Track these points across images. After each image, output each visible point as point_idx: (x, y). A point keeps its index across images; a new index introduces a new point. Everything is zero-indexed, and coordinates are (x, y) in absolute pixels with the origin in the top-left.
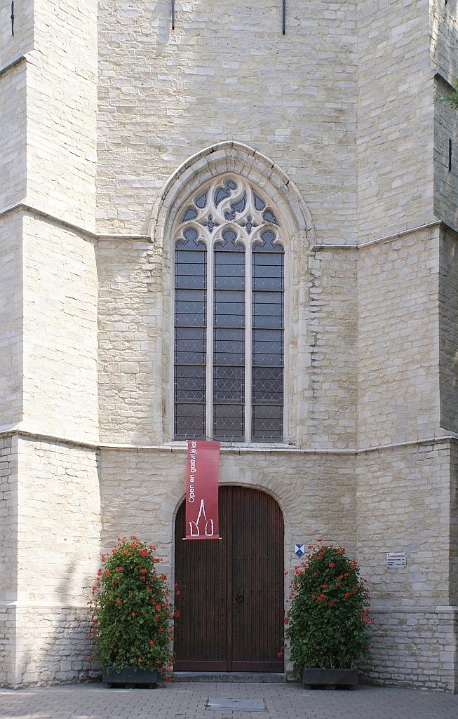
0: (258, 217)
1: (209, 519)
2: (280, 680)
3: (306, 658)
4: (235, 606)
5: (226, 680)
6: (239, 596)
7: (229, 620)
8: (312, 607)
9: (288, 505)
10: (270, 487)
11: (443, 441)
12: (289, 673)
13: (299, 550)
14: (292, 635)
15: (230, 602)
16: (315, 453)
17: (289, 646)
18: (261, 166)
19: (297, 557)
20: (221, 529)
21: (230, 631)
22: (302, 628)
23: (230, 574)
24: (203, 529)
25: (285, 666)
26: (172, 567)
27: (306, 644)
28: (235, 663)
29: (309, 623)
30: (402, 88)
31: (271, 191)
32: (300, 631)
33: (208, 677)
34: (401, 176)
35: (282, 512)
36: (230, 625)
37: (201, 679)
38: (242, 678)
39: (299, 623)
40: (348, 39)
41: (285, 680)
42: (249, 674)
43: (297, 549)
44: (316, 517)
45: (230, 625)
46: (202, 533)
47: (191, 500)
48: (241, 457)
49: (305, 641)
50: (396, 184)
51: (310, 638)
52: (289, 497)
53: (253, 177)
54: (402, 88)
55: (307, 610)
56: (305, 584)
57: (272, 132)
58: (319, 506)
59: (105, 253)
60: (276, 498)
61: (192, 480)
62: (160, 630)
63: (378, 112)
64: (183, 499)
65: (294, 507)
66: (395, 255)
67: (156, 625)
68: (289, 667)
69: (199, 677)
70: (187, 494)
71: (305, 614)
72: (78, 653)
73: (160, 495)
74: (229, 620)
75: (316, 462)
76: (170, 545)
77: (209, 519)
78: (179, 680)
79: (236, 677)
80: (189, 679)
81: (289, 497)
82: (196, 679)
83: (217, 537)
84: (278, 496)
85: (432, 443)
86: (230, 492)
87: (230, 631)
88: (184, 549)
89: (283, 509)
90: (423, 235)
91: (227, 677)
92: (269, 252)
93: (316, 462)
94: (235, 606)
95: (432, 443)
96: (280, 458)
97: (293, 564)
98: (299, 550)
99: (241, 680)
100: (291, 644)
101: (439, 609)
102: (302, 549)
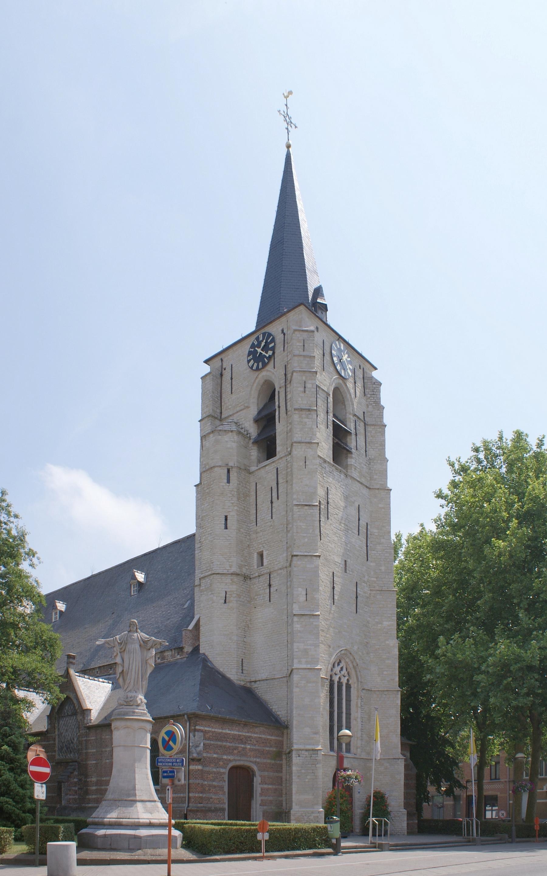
0: (346, 674)
11: (402, 759)
18: (351, 658)
30: (387, 642)
31: (351, 666)
34: (387, 671)
40: (369, 619)
50: (385, 673)
53: (347, 660)
54: (387, 642)
57: (38, 642)
59: (90, 747)
63: (378, 647)
66: (385, 696)
72: (360, 698)
85: (398, 759)
90: (395, 692)
92: (348, 686)
95: (398, 759)
101: (401, 810)
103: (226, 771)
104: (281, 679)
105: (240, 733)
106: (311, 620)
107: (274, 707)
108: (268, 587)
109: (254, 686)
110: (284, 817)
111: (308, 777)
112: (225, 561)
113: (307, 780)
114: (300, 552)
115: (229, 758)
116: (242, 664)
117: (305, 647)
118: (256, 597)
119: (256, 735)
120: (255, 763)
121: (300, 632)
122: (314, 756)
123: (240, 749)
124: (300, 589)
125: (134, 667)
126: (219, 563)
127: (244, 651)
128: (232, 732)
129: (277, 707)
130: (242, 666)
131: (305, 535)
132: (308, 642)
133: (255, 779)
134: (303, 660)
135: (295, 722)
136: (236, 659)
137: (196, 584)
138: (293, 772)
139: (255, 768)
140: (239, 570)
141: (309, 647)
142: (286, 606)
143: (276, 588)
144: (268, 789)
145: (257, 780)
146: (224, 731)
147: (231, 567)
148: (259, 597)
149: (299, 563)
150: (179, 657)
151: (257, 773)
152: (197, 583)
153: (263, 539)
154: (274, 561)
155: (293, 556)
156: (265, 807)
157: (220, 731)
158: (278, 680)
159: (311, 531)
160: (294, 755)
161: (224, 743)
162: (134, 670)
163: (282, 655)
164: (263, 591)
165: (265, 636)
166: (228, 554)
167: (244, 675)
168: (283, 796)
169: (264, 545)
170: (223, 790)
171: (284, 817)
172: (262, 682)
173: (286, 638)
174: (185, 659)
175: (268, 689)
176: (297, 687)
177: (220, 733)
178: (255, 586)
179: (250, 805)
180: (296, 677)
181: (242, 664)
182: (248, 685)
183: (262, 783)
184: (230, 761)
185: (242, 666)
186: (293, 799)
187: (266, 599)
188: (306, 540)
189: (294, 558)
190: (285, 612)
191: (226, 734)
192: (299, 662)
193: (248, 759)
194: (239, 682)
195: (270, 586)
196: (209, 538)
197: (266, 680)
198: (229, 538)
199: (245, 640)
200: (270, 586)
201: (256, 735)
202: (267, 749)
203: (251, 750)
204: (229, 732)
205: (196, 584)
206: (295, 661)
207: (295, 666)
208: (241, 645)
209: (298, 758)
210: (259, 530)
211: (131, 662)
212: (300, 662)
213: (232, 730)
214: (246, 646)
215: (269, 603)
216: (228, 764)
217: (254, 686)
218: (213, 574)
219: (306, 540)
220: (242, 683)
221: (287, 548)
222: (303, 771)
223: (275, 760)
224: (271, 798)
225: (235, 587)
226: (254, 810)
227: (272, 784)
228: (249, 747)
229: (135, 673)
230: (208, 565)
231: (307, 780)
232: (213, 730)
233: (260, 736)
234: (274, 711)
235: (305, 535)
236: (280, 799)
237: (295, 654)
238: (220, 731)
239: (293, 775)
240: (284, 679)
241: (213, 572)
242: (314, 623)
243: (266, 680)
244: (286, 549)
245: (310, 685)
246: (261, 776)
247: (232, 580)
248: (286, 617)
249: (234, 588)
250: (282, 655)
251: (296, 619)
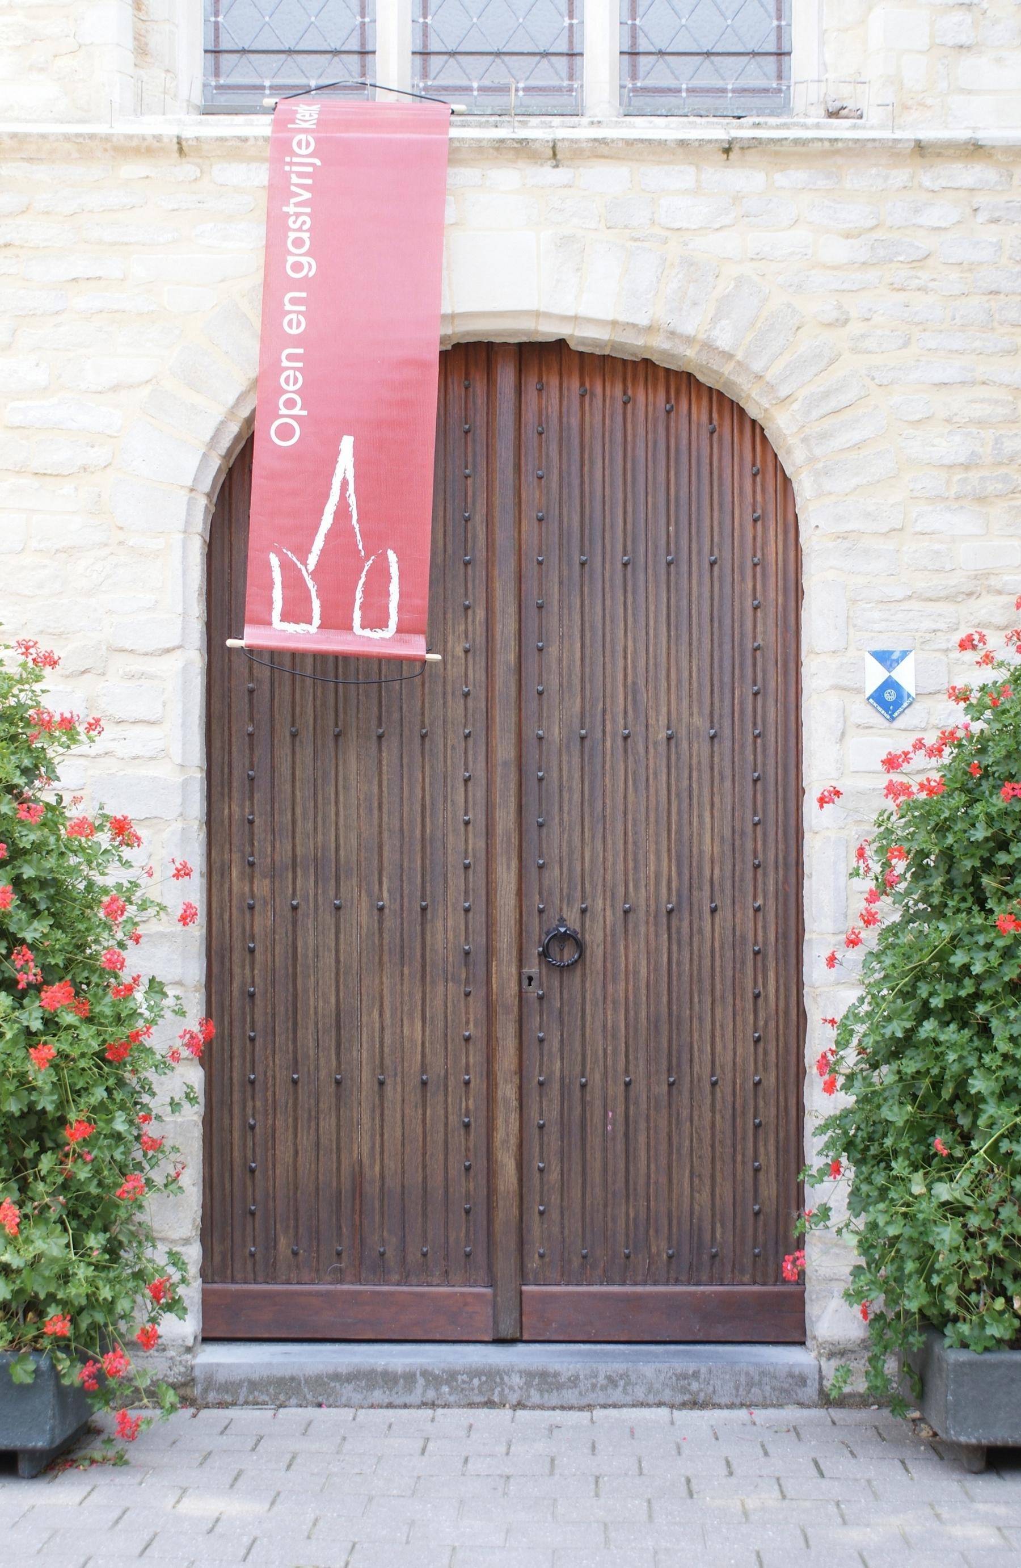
1: (376, 542)
2: (788, 1390)
3: (952, 1290)
4: (534, 991)
5: (486, 1393)
6: (563, 938)
7: (506, 1060)
8: (988, 987)
9: (824, 436)
10: (724, 340)
12: (837, 1352)
13: (890, 684)
14: (864, 1146)
15: (505, 974)
16: (975, 150)
17: (840, 1215)
19: (875, 717)
20: (434, 621)
21: (507, 1127)
22: (925, 1119)
23: (505, 819)
24: (348, 601)
25: (811, 1310)
26: (185, 784)
27: (954, 1210)
28: (533, 1295)
29: (978, 1085)
32: (920, 1132)
33: (388, 1379)
35: (787, 481)
36: (507, 1091)
37: (347, 1391)
38: (574, 1381)
39: (908, 1086)
41: (811, 1392)
42: (614, 1360)
43: (875, 675)
44: (981, 500)
45: (507, 1091)
46: (336, 619)
47: (285, 432)
48: (562, 175)
49: (944, 1191)
51: (979, 1179)
52: (827, 395)
55: (957, 1011)
56: (948, 856)
58: (997, 441)
60: (756, 404)
61: (294, 323)
62: (72, 1137)
64: (245, 413)
65: (857, 446)
67: (47, 1103)
68: (834, 1317)
69: (336, 1377)
70: (265, 383)
71: (950, 1034)
73: (115, 388)
74: (506, 1060)
75: (979, 200)
76: (173, 664)
77: (376, 542)
78: (232, 1393)
79: (544, 1375)
80: (281, 1391)
81: (827, 395)
82: (320, 1392)
83: (416, 647)
84: (771, 388)
86: (506, 377)
87: (507, 1127)
88: (261, 716)
89: (795, 460)
91: (492, 1376)
93: (979, 200)
94: (534, 991)
96: (781, 179)
97: (858, 768)
98: (890, 684)
99: (570, 1396)
100: (858, 1201)
102: (905, 675)
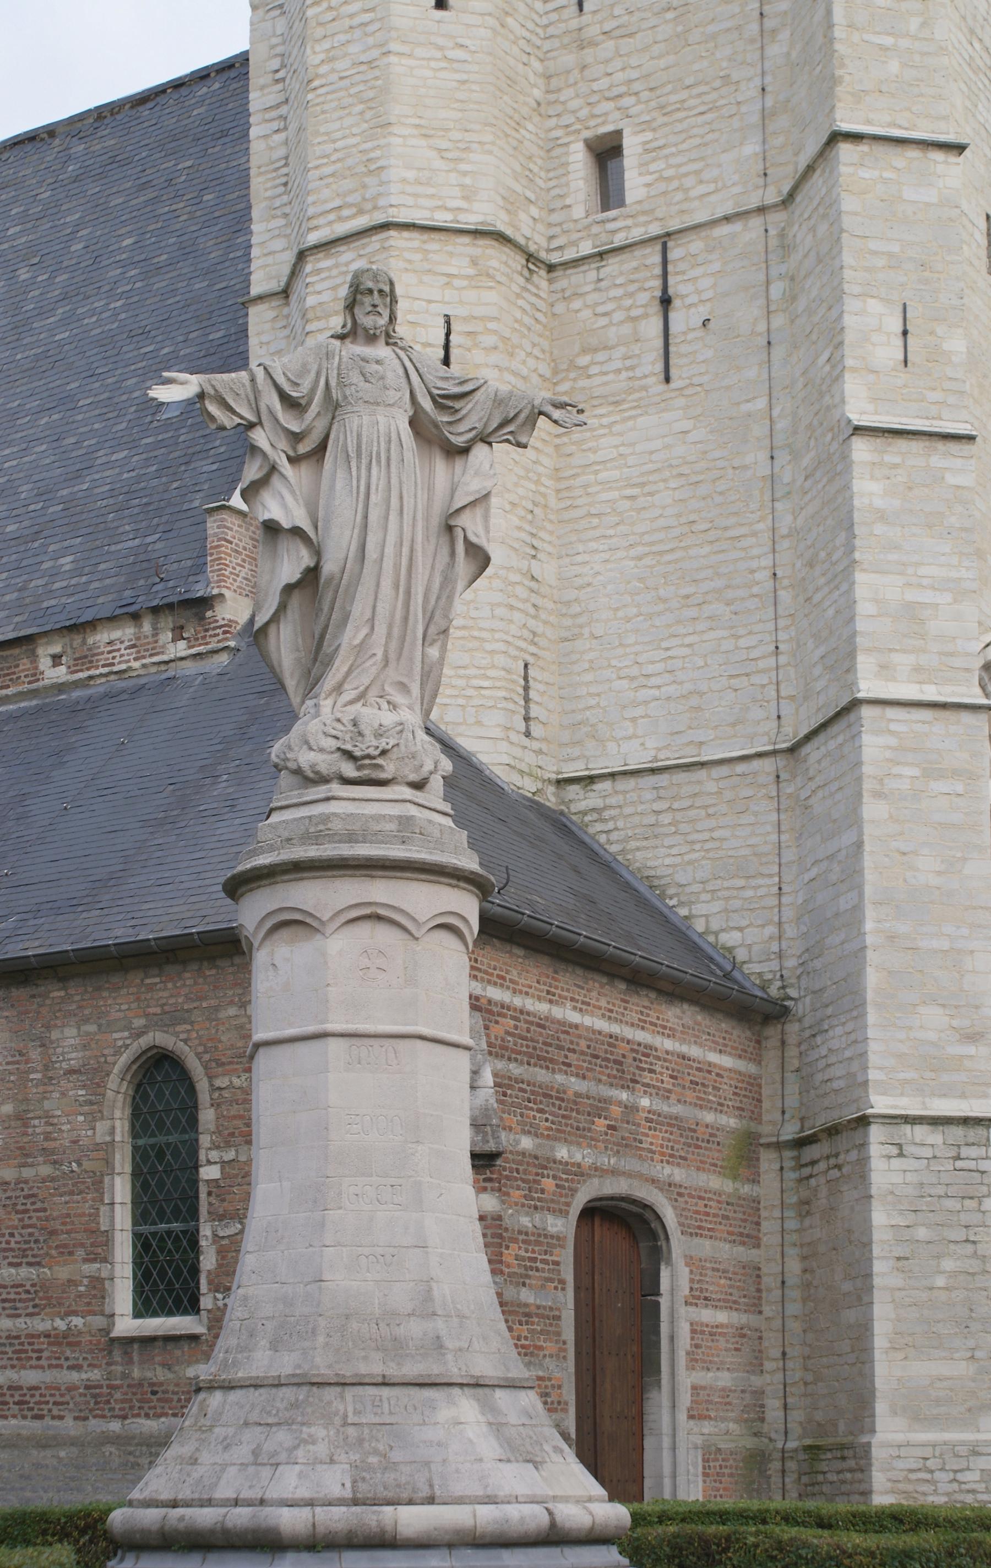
103: (562, 1226)
104: (740, 768)
105: (615, 1029)
106: (937, 461)
107: (699, 909)
108: (656, 308)
109: (581, 801)
110: (776, 1480)
111: (948, 1264)
112: (439, 164)
113: (940, 1282)
114: (869, 122)
115: (578, 1157)
116: (526, 688)
117: (911, 596)
118: (584, 360)
119: (669, 1044)
120: (668, 1186)
121: (882, 516)
122: (973, 1152)
123: (616, 1110)
124: (874, 306)
125: (389, 550)
126: (411, 175)
127: (532, 623)
128: (588, 1021)
129: (716, 907)
130: (527, 700)
131: (888, 41)
132: (922, 571)
133: (665, 1274)
134: (903, 661)
135: (872, 979)
136: (501, 660)
137: (255, 291)
138: (877, 1236)
139: (670, 1216)
140: (503, 216)
141: (927, 597)
142: (761, 403)
143: (703, 311)
144: (714, 1332)
145: (675, 1279)
146: (558, 1012)
147: (465, 198)
148: (601, 356)
149: (865, 174)
150: (181, 649)
151: (678, 1245)
152: (265, 274)
153: (620, 77)
154: (689, 182)
155: (836, 137)
156: (707, 1427)
157: (543, 1008)
158: (724, 770)
159: (914, 24)
160: (875, 1150)
161: (560, 1078)
162: (388, 564)
163: (743, 643)
164: (627, 329)
165: (640, 550)
166: (456, 135)
167: (536, 745)
168: (768, 1365)
169: (627, 101)
170: (558, 1334)
171: (776, 1480)
172: (622, 784)
173: (767, 562)
174: (224, 658)
175: (666, 819)
176: (878, 795)
177: (542, 1023)
178: (577, 304)
179: (641, 1414)
180: (876, 740)
181: (526, 688)
182: (550, 798)
183: (698, 1298)
184: (578, 1173)
185: (527, 700)
186: (879, 1383)
187: (647, 369)
188: (894, 66)
189: (845, 150)
190: (759, 430)
191: (567, 1028)
192: (883, 667)
193: (644, 1168)
194: (516, 779)
195: (666, 301)
196: (353, 49)
197: (653, 771)
198: (459, 54)
199: (536, 568)
200: (666, 301)
201: (669, 1044)
202: (709, 1117)
203: (655, 1119)
204: (574, 1017)
205: (255, 291)
206: (865, 663)
207: (866, 689)
208: (519, 590)
209: (897, 1163)
210: (593, 31)
211: (375, 515)
212: (885, 669)
213: (583, 1007)
214: (539, 601)
215: (663, 387)
216: (574, 1191)
217: (582, 806)
218: (385, 226)
219: (894, 66)
220: (529, 786)
221: (765, 116)
222: (922, 1233)
223: (735, 1178)
224: (724, 1379)
225: (491, 296)
226: (666, 1442)
227: (731, 1305)
228: (645, 1102)
229: (396, 586)
230: (347, 184)
231: (940, 1282)
232: (518, 1001)
233: (684, 1049)
234: (699, 926)
235: (888, 41)
236: (757, 1381)
237: (860, 625)
238: (543, 1008)
239: (876, 1251)
240: (756, 764)
241: (380, 218)
242: (951, 479)
243: (653, 771)
244: (755, 118)
245: (939, 786)
246: (690, 1261)
247: (474, 262)
248: (763, 456)
249: (489, 300)
250: (743, 643)
251: (861, 449)
